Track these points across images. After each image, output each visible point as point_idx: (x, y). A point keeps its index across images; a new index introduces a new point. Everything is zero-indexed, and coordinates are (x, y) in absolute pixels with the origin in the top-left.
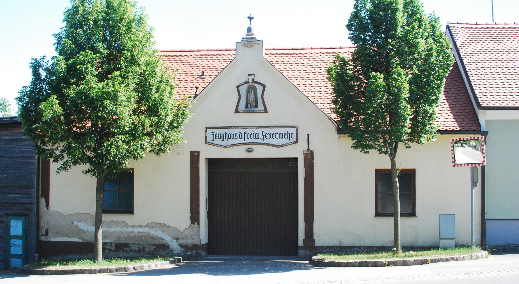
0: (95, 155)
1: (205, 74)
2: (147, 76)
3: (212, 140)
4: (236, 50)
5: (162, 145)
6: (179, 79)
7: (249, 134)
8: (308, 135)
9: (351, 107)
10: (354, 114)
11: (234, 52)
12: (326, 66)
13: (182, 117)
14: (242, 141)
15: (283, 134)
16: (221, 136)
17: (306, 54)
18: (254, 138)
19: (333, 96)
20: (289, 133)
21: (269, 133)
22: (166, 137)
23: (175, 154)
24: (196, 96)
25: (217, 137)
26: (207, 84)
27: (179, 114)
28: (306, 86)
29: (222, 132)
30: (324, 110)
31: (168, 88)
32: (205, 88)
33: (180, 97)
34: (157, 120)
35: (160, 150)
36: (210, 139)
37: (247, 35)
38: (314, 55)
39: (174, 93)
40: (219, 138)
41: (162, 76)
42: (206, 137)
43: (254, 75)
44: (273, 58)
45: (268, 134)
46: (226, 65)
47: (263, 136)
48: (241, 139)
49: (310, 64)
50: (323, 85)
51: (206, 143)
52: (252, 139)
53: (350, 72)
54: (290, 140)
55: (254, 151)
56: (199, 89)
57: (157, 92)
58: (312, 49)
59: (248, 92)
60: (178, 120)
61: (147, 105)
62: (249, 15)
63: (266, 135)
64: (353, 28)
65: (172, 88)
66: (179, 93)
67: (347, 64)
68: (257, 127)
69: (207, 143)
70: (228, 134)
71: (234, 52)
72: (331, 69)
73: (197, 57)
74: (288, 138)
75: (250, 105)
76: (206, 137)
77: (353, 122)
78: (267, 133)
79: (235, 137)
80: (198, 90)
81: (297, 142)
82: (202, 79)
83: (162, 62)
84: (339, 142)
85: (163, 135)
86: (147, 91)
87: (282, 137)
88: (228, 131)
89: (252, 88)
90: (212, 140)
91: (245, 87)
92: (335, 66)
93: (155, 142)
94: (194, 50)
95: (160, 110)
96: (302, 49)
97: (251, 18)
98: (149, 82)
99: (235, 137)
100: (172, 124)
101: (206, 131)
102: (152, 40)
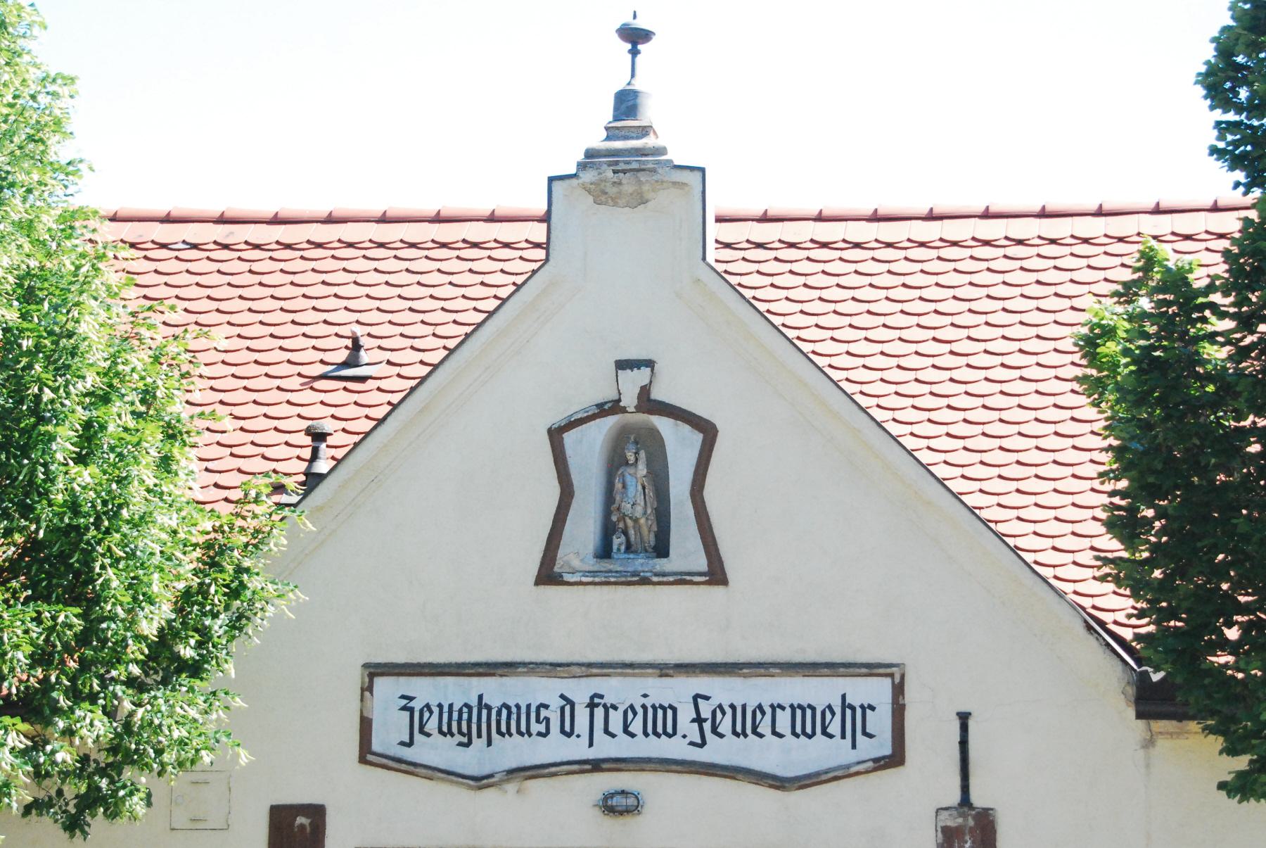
0: (1189, 415)
1: (364, 357)
2: (24, 361)
3: (402, 744)
4: (546, 218)
5: (102, 772)
6: (212, 383)
7: (615, 708)
8: (964, 718)
9: (1221, 557)
10: (1242, 599)
11: (538, 232)
12: (1082, 318)
13: (227, 608)
14: (577, 749)
15: (813, 709)
16: (455, 716)
17: (955, 244)
18: (646, 734)
19: (1112, 494)
20: (853, 709)
21: (733, 707)
22: (127, 726)
23: (181, 820)
24: (312, 480)
25: (432, 726)
26: (379, 413)
27: (213, 589)
28: (953, 430)
29: (457, 691)
30: (1060, 572)
31: (152, 435)
32: (367, 434)
33: (216, 485)
34: (79, 624)
35: (90, 800)
36: (387, 737)
37: (612, 133)
38: (1001, 252)
39: (183, 463)
40: (735, 733)
41: (115, 363)
42: (366, 726)
43: (650, 364)
44: (764, 268)
45: (729, 711)
46: (491, 305)
47: (699, 720)
48: (569, 735)
49: (975, 306)
50: (1052, 428)
51: (363, 760)
52: (633, 735)
53: (1217, 354)
54: (854, 746)
55: (646, 810)
56: (330, 440)
57: (81, 460)
58: (987, 215)
59: (615, 463)
60: (208, 622)
61: (21, 530)
62: (628, 19)
63: (719, 715)
64: (1243, 94)
65: (172, 434)
66: (211, 465)
67: (1202, 307)
68: (665, 670)
69: (370, 757)
70: (495, 703)
71: (538, 232)
72: (1108, 332)
73: (319, 253)
74: (843, 737)
75: (623, 538)
76: (366, 726)
77: (1232, 647)
78: (720, 706)
79: (536, 727)
80: (323, 446)
81: (895, 759)
82: (350, 385)
83: (113, 278)
84: (1148, 766)
85: (110, 713)
86: (25, 451)
87: (809, 730)
88: (496, 691)
89: (636, 442)
90: (402, 744)
91: (599, 432)
92: (1131, 318)
93: (65, 756)
94: (306, 216)
95: (103, 567)
96: (931, 217)
97: (635, 37)
98: (38, 398)
99: (536, 727)
100: (170, 648)
101: (368, 689)
102: (60, 151)
